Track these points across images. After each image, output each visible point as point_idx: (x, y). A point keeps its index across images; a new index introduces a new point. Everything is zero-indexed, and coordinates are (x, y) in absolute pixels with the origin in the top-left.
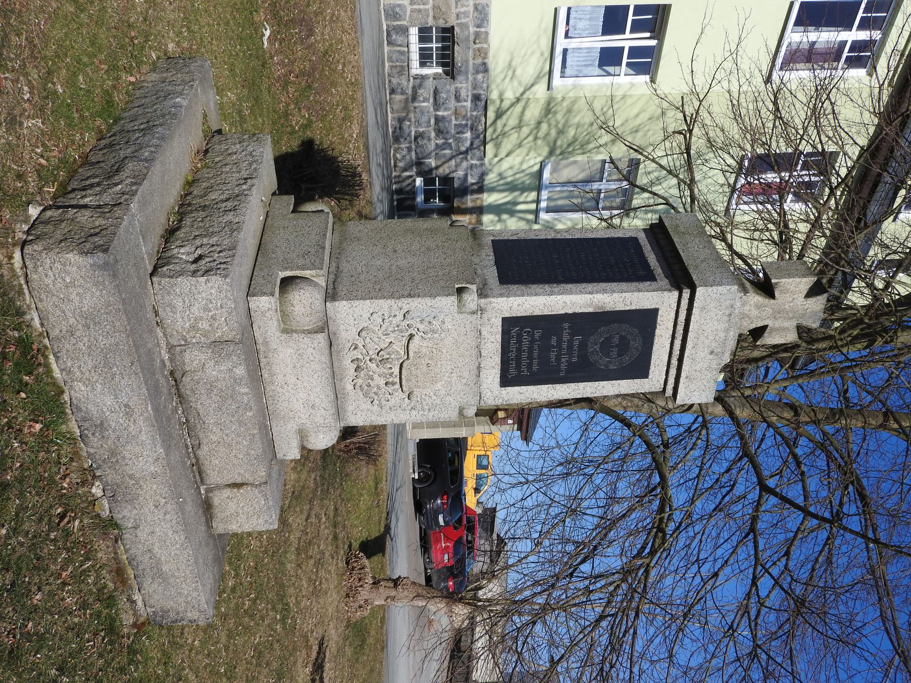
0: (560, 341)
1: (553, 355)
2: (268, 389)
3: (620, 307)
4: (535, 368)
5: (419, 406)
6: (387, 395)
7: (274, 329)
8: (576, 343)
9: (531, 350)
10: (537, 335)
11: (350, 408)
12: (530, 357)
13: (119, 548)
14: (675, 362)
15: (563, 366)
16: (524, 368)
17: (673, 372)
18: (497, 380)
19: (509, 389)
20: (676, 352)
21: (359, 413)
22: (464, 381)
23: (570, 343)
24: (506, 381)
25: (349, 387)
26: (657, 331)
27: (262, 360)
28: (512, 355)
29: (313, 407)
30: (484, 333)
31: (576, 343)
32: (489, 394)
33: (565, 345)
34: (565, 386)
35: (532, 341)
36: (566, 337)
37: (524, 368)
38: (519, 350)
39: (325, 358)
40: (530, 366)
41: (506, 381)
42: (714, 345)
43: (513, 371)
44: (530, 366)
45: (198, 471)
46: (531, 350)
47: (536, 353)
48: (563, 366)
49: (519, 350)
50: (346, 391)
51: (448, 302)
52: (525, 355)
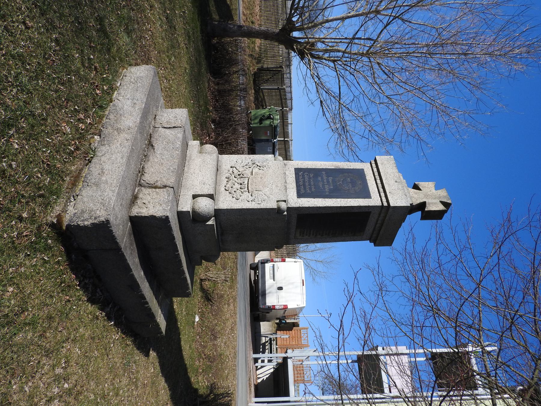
0: (322, 178)
1: (321, 185)
2: (185, 175)
3: (346, 167)
4: (313, 190)
5: (256, 200)
6: (241, 194)
7: (195, 152)
8: (330, 180)
9: (309, 181)
10: (311, 176)
11: (221, 199)
12: (310, 185)
13: (86, 168)
14: (381, 190)
15: (327, 190)
16: (308, 190)
17: (383, 194)
18: (296, 194)
19: (302, 199)
20: (380, 185)
21: (225, 202)
22: (279, 188)
23: (328, 182)
24: (300, 195)
25: (223, 189)
26: (367, 178)
27: (187, 163)
28: (301, 183)
29: (204, 184)
30: (287, 173)
31: (330, 180)
32: (292, 201)
33: (325, 181)
34: (330, 200)
35: (310, 178)
36: (325, 178)
37: (308, 190)
38: (304, 181)
39: (214, 178)
40: (310, 189)
41: (300, 195)
42: (395, 178)
43: (302, 191)
44: (310, 189)
45: (142, 172)
46: (309, 181)
47: (312, 183)
48: (327, 190)
49: (304, 181)
50: (220, 191)
51: (271, 156)
52: (307, 184)
